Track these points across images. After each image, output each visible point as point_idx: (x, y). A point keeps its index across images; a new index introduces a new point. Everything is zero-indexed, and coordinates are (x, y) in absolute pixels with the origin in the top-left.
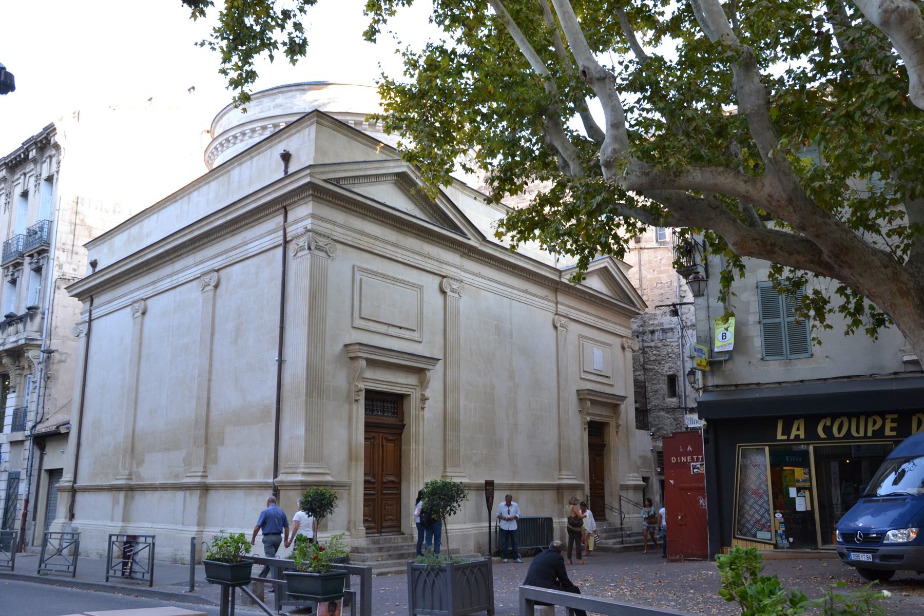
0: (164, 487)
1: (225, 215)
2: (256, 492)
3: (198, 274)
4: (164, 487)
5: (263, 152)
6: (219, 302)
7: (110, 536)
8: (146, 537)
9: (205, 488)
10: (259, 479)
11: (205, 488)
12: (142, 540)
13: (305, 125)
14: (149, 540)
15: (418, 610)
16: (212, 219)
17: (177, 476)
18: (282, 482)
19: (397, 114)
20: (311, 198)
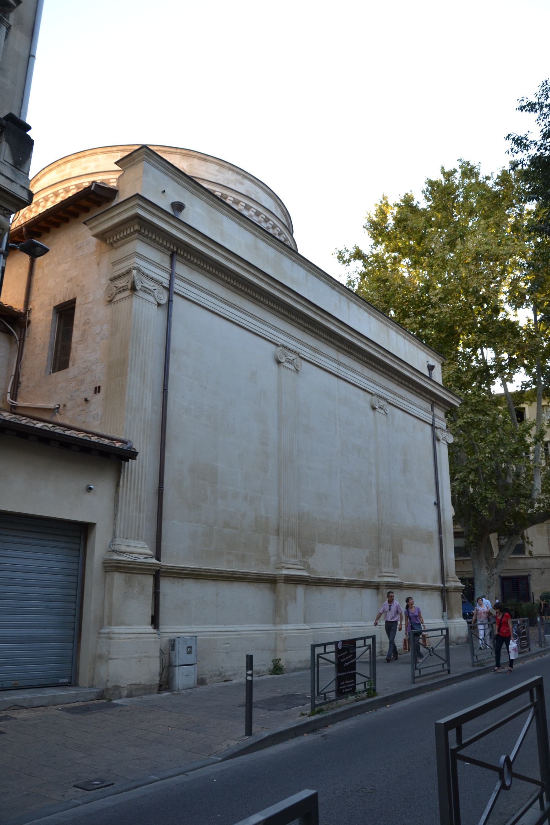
0: (350, 584)
1: (413, 374)
2: (429, 592)
3: (280, 342)
4: (350, 584)
5: (412, 343)
6: (38, 274)
7: (313, 647)
8: (364, 639)
9: (158, 575)
10: (430, 583)
11: (158, 575)
12: (359, 643)
13: (436, 358)
14: (369, 641)
15: (241, 679)
16: (219, 251)
17: (360, 574)
18: (167, 567)
19: (473, 408)
20: (136, 235)
